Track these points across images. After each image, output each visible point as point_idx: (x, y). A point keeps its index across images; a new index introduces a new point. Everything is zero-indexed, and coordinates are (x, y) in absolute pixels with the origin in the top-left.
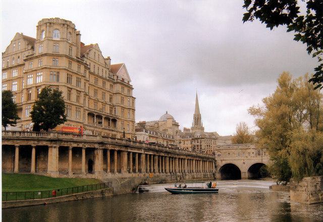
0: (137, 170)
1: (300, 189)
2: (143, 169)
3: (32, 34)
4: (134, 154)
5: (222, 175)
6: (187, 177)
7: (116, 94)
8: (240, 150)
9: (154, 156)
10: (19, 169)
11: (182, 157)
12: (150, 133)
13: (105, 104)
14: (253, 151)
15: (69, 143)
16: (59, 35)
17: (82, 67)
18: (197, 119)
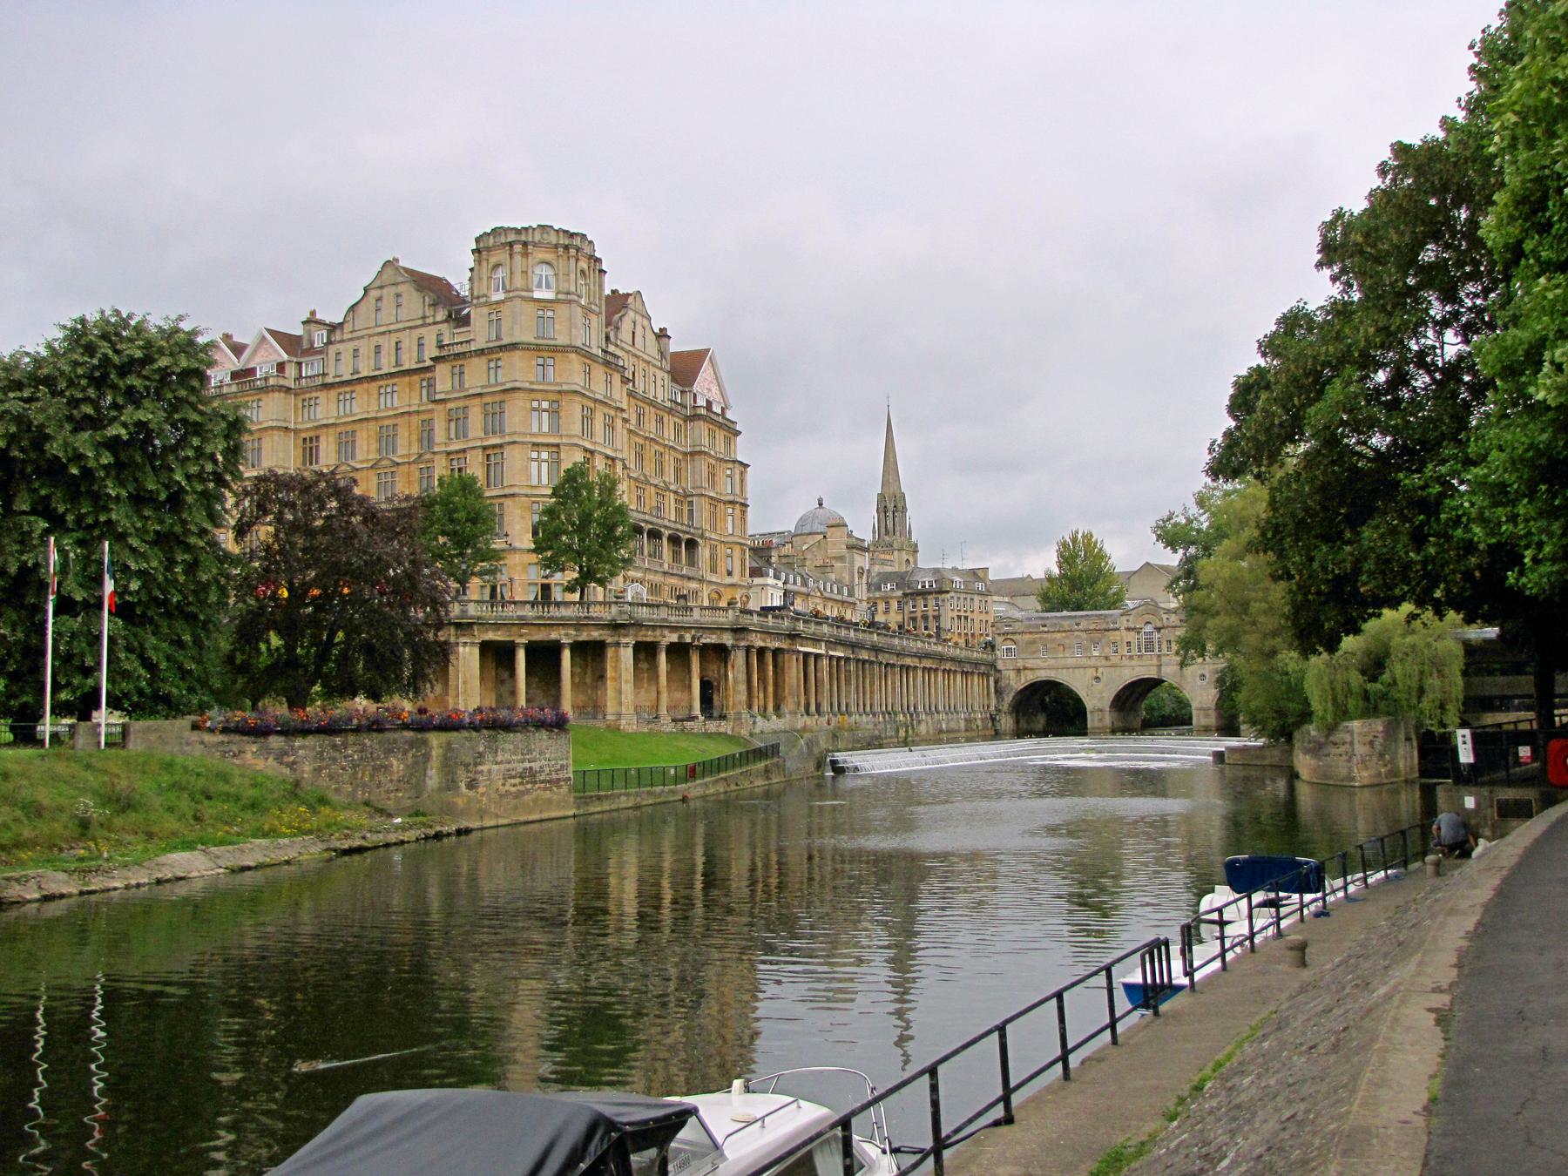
1: (1334, 750)
3: (457, 271)
4: (806, 655)
5: (1017, 722)
6: (923, 729)
7: (692, 454)
8: (1084, 635)
9: (847, 659)
10: (528, 700)
11: (908, 661)
13: (662, 490)
14: (1132, 636)
15: (658, 632)
16: (552, 280)
17: (616, 378)
18: (891, 507)
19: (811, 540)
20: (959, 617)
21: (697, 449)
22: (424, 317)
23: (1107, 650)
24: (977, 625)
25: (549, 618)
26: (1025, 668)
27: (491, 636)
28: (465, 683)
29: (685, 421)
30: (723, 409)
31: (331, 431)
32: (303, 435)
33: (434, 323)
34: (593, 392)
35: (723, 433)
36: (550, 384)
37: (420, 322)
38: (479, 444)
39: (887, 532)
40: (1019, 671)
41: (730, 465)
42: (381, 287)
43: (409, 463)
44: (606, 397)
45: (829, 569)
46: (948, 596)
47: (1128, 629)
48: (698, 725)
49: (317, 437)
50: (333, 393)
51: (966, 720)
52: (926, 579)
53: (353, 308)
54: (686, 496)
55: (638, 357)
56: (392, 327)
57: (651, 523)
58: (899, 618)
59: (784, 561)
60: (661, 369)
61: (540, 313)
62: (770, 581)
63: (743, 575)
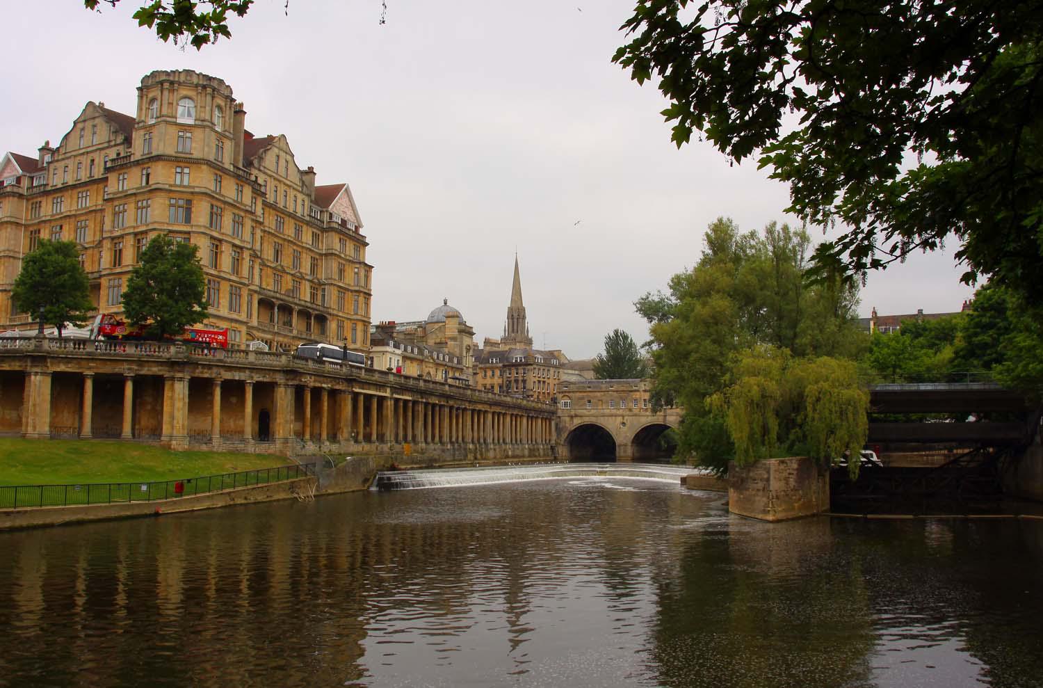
0: (374, 437)
2: (389, 435)
3: (127, 105)
4: (368, 398)
7: (326, 255)
9: (415, 403)
11: (479, 407)
12: (405, 350)
16: (193, 111)
17: (248, 191)
18: (517, 316)
19: (436, 326)
20: (539, 382)
21: (330, 251)
22: (109, 141)
23: (631, 404)
24: (551, 385)
25: (115, 355)
26: (576, 416)
27: (62, 368)
28: (34, 405)
29: (322, 232)
30: (356, 227)
31: (48, 225)
32: (31, 229)
33: (115, 145)
34: (223, 196)
35: (310, 230)
36: (185, 187)
37: (106, 145)
38: (132, 231)
39: (513, 331)
40: (572, 417)
41: (358, 266)
42: (84, 121)
43: (93, 247)
44: (237, 201)
45: (444, 345)
46: (532, 367)
47: (645, 391)
48: (252, 447)
49: (39, 231)
50: (50, 199)
51: (530, 449)
52: (518, 356)
53: (66, 137)
54: (320, 284)
55: (280, 181)
56: (89, 149)
57: (282, 300)
58: (500, 381)
59: (408, 337)
60: (301, 192)
61: (179, 170)
62: (390, 349)
63: (364, 342)
